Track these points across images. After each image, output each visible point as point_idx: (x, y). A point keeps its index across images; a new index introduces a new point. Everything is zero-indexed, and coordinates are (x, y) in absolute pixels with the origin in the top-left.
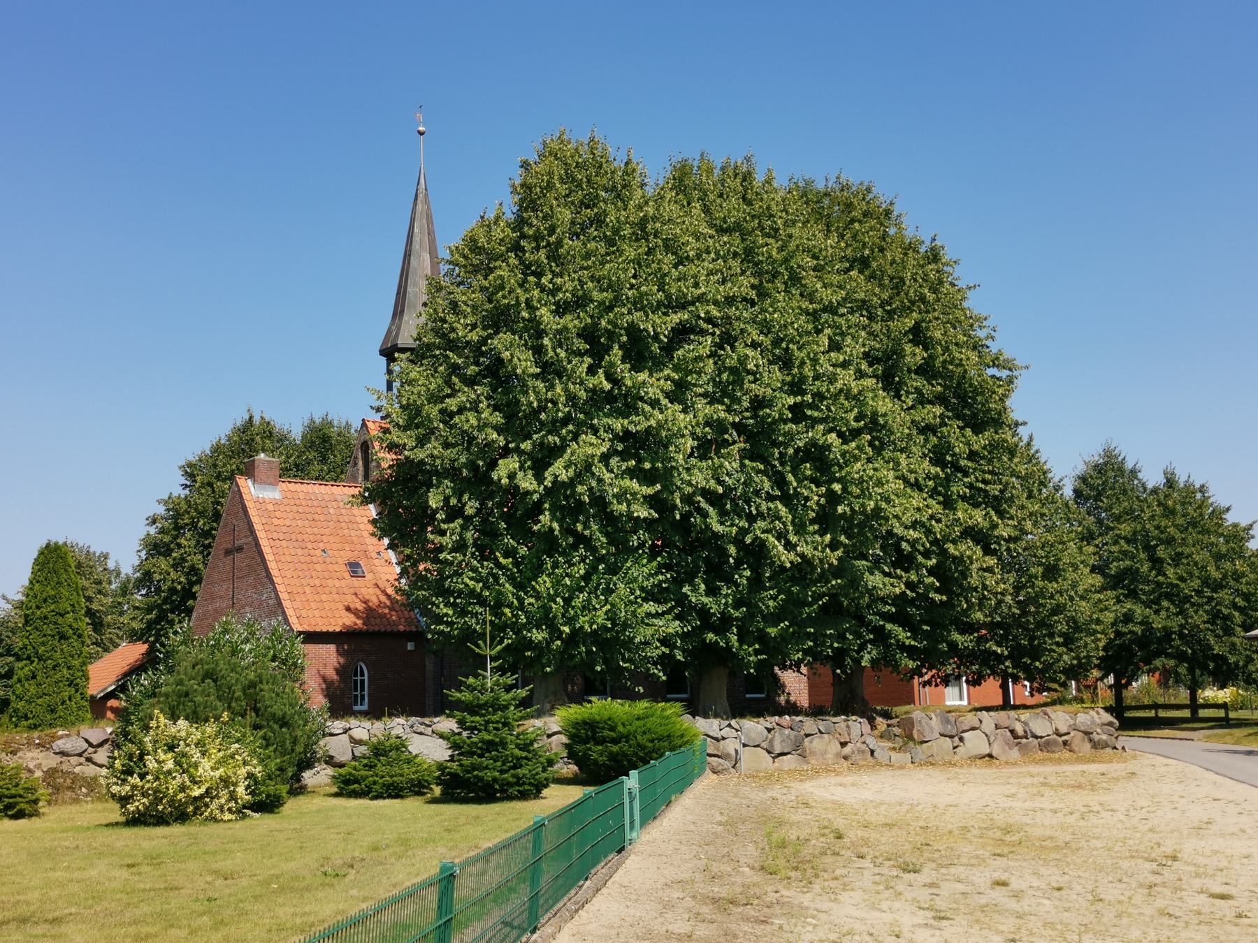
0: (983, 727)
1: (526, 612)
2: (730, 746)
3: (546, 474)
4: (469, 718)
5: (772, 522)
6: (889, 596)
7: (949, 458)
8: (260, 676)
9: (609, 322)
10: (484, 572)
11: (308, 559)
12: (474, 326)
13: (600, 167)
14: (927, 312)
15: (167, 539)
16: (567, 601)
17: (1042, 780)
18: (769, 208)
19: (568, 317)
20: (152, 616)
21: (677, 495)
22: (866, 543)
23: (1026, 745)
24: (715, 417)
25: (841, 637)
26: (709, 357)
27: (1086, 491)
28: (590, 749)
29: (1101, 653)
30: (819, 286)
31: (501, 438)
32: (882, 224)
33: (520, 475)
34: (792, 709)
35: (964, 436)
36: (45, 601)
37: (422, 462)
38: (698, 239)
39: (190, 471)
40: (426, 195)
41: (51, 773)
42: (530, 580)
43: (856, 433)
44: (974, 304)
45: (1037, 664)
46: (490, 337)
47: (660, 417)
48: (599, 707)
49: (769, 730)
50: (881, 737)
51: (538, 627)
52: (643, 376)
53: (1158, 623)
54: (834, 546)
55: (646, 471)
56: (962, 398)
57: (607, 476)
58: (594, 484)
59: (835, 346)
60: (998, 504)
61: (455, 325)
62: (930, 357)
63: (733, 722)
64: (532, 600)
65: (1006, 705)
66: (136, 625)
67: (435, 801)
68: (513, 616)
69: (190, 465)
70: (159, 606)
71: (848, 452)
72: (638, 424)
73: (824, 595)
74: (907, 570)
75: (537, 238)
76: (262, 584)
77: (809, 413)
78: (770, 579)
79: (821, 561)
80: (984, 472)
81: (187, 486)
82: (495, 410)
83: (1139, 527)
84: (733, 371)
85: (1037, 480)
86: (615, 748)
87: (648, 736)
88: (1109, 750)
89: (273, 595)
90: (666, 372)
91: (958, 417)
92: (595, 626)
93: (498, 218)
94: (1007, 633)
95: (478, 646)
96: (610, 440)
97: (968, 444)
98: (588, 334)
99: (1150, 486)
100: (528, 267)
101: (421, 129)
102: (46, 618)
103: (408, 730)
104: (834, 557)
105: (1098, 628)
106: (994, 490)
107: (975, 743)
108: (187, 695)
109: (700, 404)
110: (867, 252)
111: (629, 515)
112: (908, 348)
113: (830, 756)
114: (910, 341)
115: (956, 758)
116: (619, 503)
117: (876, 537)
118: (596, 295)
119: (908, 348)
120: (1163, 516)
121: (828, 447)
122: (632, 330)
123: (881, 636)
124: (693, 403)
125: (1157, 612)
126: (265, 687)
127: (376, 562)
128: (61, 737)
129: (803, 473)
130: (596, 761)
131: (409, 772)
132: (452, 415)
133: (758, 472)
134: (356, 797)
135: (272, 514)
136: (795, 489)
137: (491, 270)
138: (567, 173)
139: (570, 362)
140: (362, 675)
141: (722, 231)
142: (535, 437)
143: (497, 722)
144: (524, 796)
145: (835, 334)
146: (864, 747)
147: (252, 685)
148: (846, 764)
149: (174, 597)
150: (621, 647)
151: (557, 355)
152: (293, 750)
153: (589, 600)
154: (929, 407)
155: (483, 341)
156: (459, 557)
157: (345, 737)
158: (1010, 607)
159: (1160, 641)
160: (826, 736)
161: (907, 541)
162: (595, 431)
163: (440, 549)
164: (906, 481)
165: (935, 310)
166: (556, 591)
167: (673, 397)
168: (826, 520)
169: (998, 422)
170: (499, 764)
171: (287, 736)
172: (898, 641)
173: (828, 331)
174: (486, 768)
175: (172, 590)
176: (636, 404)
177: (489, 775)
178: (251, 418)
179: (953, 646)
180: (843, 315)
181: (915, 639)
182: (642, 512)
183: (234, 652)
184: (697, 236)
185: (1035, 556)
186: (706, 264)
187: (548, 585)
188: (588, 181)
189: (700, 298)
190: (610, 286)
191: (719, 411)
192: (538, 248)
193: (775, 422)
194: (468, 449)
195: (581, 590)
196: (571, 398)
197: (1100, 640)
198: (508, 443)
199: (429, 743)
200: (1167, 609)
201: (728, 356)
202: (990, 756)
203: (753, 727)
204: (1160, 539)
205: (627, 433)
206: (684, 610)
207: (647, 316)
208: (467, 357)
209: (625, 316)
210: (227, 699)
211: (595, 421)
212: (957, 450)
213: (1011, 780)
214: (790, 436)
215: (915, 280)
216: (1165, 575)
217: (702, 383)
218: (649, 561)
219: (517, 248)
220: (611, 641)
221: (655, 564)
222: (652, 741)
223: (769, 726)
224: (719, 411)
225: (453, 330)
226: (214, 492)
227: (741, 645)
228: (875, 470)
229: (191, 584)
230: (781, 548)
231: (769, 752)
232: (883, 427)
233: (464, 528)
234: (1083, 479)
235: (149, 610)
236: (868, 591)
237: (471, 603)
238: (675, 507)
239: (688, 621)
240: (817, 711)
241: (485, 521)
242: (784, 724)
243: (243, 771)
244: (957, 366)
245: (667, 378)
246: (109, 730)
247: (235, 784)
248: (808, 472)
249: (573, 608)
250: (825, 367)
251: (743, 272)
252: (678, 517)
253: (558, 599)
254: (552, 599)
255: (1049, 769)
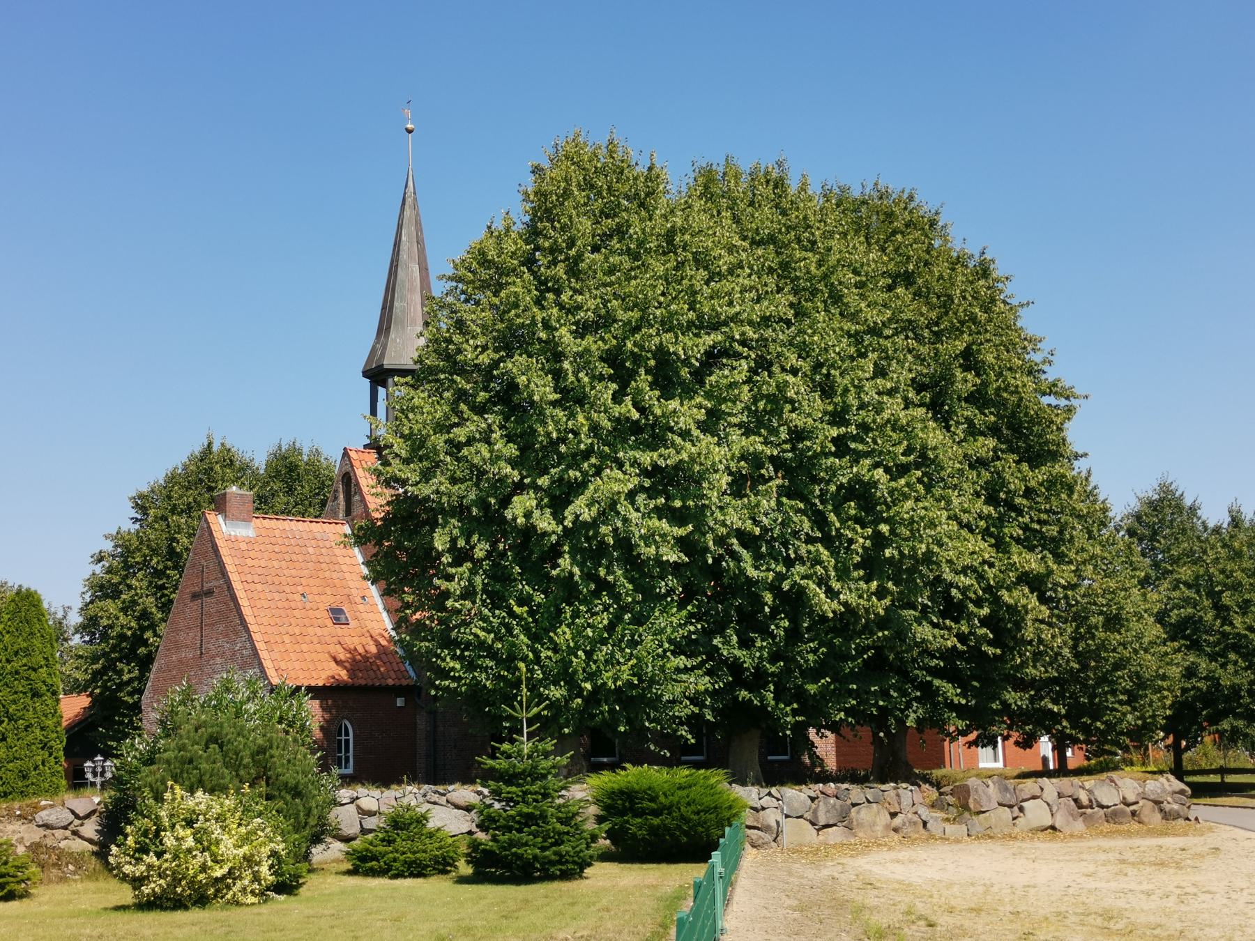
0: (1045, 795)
1: (542, 667)
2: (771, 817)
3: (566, 513)
4: (505, 789)
5: (812, 566)
6: (939, 650)
7: (1002, 495)
8: (270, 740)
9: (635, 344)
10: (495, 621)
11: (286, 604)
12: (485, 348)
13: (622, 173)
14: (979, 333)
15: (116, 580)
16: (589, 654)
17: (1118, 856)
18: (805, 218)
19: (590, 339)
20: (97, 666)
21: (709, 536)
22: (916, 591)
23: (1091, 816)
24: (752, 449)
25: (884, 694)
26: (744, 383)
27: (1141, 530)
28: (627, 822)
29: (1168, 712)
30: (863, 305)
31: (516, 473)
32: (926, 236)
33: (537, 513)
34: (824, 778)
35: (1019, 471)
36: (16, 653)
37: (427, 499)
38: (730, 252)
39: (142, 504)
40: (415, 199)
41: (35, 848)
42: (547, 631)
43: (903, 470)
44: (1028, 322)
45: (1098, 724)
46: (501, 360)
47: (693, 450)
48: (632, 775)
49: (813, 799)
50: (933, 806)
51: (556, 683)
52: (674, 404)
53: (1227, 679)
54: (881, 593)
55: (675, 509)
56: (1016, 427)
57: (634, 516)
58: (619, 524)
59: (880, 372)
60: (1055, 547)
61: (465, 346)
62: (983, 383)
63: (774, 790)
64: (550, 653)
65: (1062, 770)
66: (79, 675)
67: (463, 880)
68: (528, 670)
69: (141, 496)
70: (105, 654)
71: (896, 489)
72: (666, 457)
73: (868, 648)
74: (957, 621)
75: (553, 250)
76: (236, 633)
77: (853, 446)
78: (809, 629)
79: (867, 610)
80: (1040, 511)
81: (137, 520)
82: (508, 442)
83: (1202, 572)
84: (770, 398)
85: (1096, 519)
86: (656, 821)
87: (693, 807)
88: (1181, 821)
89: (248, 645)
90: (699, 400)
91: (1012, 450)
92: (619, 683)
93: (508, 229)
94: (1063, 690)
95: (513, 708)
96: (636, 475)
97: (1024, 479)
98: (611, 358)
99: (1211, 525)
100: (545, 283)
101: (410, 126)
102: (17, 673)
103: (421, 799)
104: (880, 606)
105: (1165, 684)
106: (1053, 531)
107: (1036, 813)
108: (191, 761)
109: (735, 435)
110: (911, 267)
111: (658, 560)
112: (959, 374)
113: (879, 828)
114: (961, 366)
115: (1016, 830)
116: (647, 546)
117: (925, 585)
118: (620, 314)
119: (959, 374)
120: (1230, 559)
121: (875, 484)
122: (662, 354)
123: (929, 693)
124: (727, 435)
125: (1223, 666)
126: (274, 752)
127: (361, 607)
128: (44, 808)
129: (846, 513)
130: (634, 835)
131: (432, 848)
132: (459, 446)
133: (798, 511)
134: (373, 876)
135: (246, 554)
136: (838, 530)
137: (501, 286)
138: (585, 179)
139: (593, 388)
140: (347, 734)
141: (755, 243)
142: (553, 471)
143: (536, 793)
144: (566, 876)
145: (880, 358)
146: (915, 818)
147: (262, 751)
148: (896, 837)
149: (124, 644)
150: (647, 705)
151: (579, 380)
152: (306, 824)
153: (612, 654)
154: (981, 439)
155: (495, 364)
156: (468, 604)
157: (352, 807)
158: (1068, 661)
159: (1227, 699)
160: (874, 805)
161: (957, 587)
162: (620, 466)
163: (446, 595)
164: (961, 525)
165: (986, 331)
166: (576, 643)
167: (705, 427)
168: (872, 565)
169: (1054, 454)
170: (540, 840)
171: (301, 808)
172: (946, 699)
173: (873, 356)
174: (526, 844)
175: (122, 637)
176: (665, 435)
177: (529, 852)
178: (210, 444)
179: (1005, 705)
180: (887, 338)
181: (965, 697)
182: (672, 556)
183: (238, 715)
184: (731, 249)
185: (1095, 604)
186: (741, 280)
187: (568, 636)
188: (609, 188)
189: (735, 318)
190: (636, 305)
191: (755, 444)
192: (554, 263)
193: (816, 455)
194: (477, 485)
195: (604, 642)
196: (595, 429)
197: (1166, 697)
198: (523, 478)
199: (450, 812)
200: (1236, 663)
201: (765, 382)
202: (1053, 828)
203: (796, 795)
204: (1225, 585)
205: (655, 466)
206: (715, 664)
207: (677, 338)
208: (476, 383)
209: (654, 338)
210: (234, 765)
211: (621, 455)
212: (1012, 487)
213: (1084, 856)
214: (832, 471)
215: (964, 298)
216: (1231, 624)
217: (737, 413)
218: (680, 610)
219: (530, 262)
220: (635, 699)
221: (684, 613)
222: (698, 813)
223: (813, 795)
224: (755, 444)
225: (459, 351)
226: (168, 526)
227: (777, 704)
228: (925, 508)
229: (143, 629)
230: (823, 596)
231: (813, 824)
232: (933, 462)
233: (473, 572)
234: (1138, 517)
235: (95, 659)
236: (917, 644)
237: (480, 657)
238: (706, 550)
239: (718, 676)
240: (849, 775)
241: (495, 565)
242: (829, 792)
243: (265, 851)
244: (1012, 393)
245: (700, 407)
246: (97, 800)
247: (259, 864)
248: (853, 512)
249: (595, 662)
250: (870, 395)
251: (779, 290)
252: (710, 561)
253: (580, 653)
254: (573, 652)
255: (1120, 843)
